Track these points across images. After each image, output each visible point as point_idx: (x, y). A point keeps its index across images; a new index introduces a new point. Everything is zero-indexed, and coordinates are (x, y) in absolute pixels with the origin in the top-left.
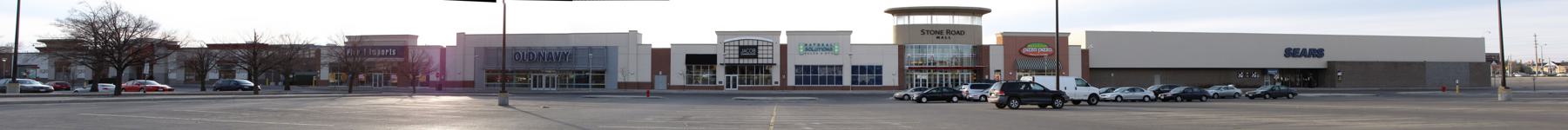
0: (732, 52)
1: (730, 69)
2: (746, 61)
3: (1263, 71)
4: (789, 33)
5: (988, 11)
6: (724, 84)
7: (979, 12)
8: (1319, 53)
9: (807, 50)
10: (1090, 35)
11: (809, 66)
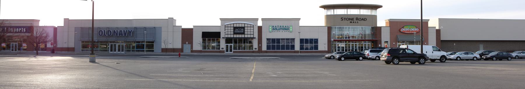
0: (229, 31)
1: (228, 40)
2: (238, 36)
5: (380, 7)
6: (225, 49)
9: (273, 29)
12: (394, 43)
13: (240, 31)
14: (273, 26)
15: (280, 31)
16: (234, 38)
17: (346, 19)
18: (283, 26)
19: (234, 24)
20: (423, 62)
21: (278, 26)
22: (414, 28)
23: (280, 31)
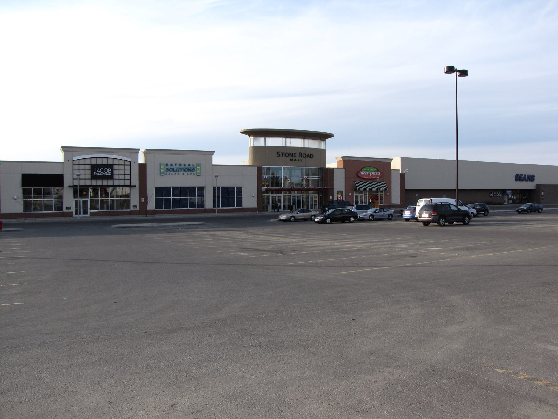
0: (82, 172)
1: (80, 191)
2: (99, 183)
3: (503, 192)
4: (148, 152)
5: (330, 136)
6: (73, 210)
7: (323, 136)
8: (531, 178)
9: (168, 170)
10: (404, 160)
11: (195, 188)
12: (350, 194)
13: (104, 173)
14: (167, 165)
15: (178, 174)
16: (91, 186)
17: (284, 154)
18: (185, 165)
19: (91, 158)
20: (443, 223)
21: (176, 164)
22: (376, 171)
23: (179, 172)
